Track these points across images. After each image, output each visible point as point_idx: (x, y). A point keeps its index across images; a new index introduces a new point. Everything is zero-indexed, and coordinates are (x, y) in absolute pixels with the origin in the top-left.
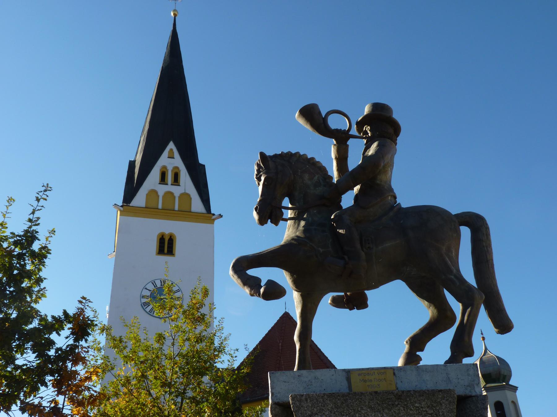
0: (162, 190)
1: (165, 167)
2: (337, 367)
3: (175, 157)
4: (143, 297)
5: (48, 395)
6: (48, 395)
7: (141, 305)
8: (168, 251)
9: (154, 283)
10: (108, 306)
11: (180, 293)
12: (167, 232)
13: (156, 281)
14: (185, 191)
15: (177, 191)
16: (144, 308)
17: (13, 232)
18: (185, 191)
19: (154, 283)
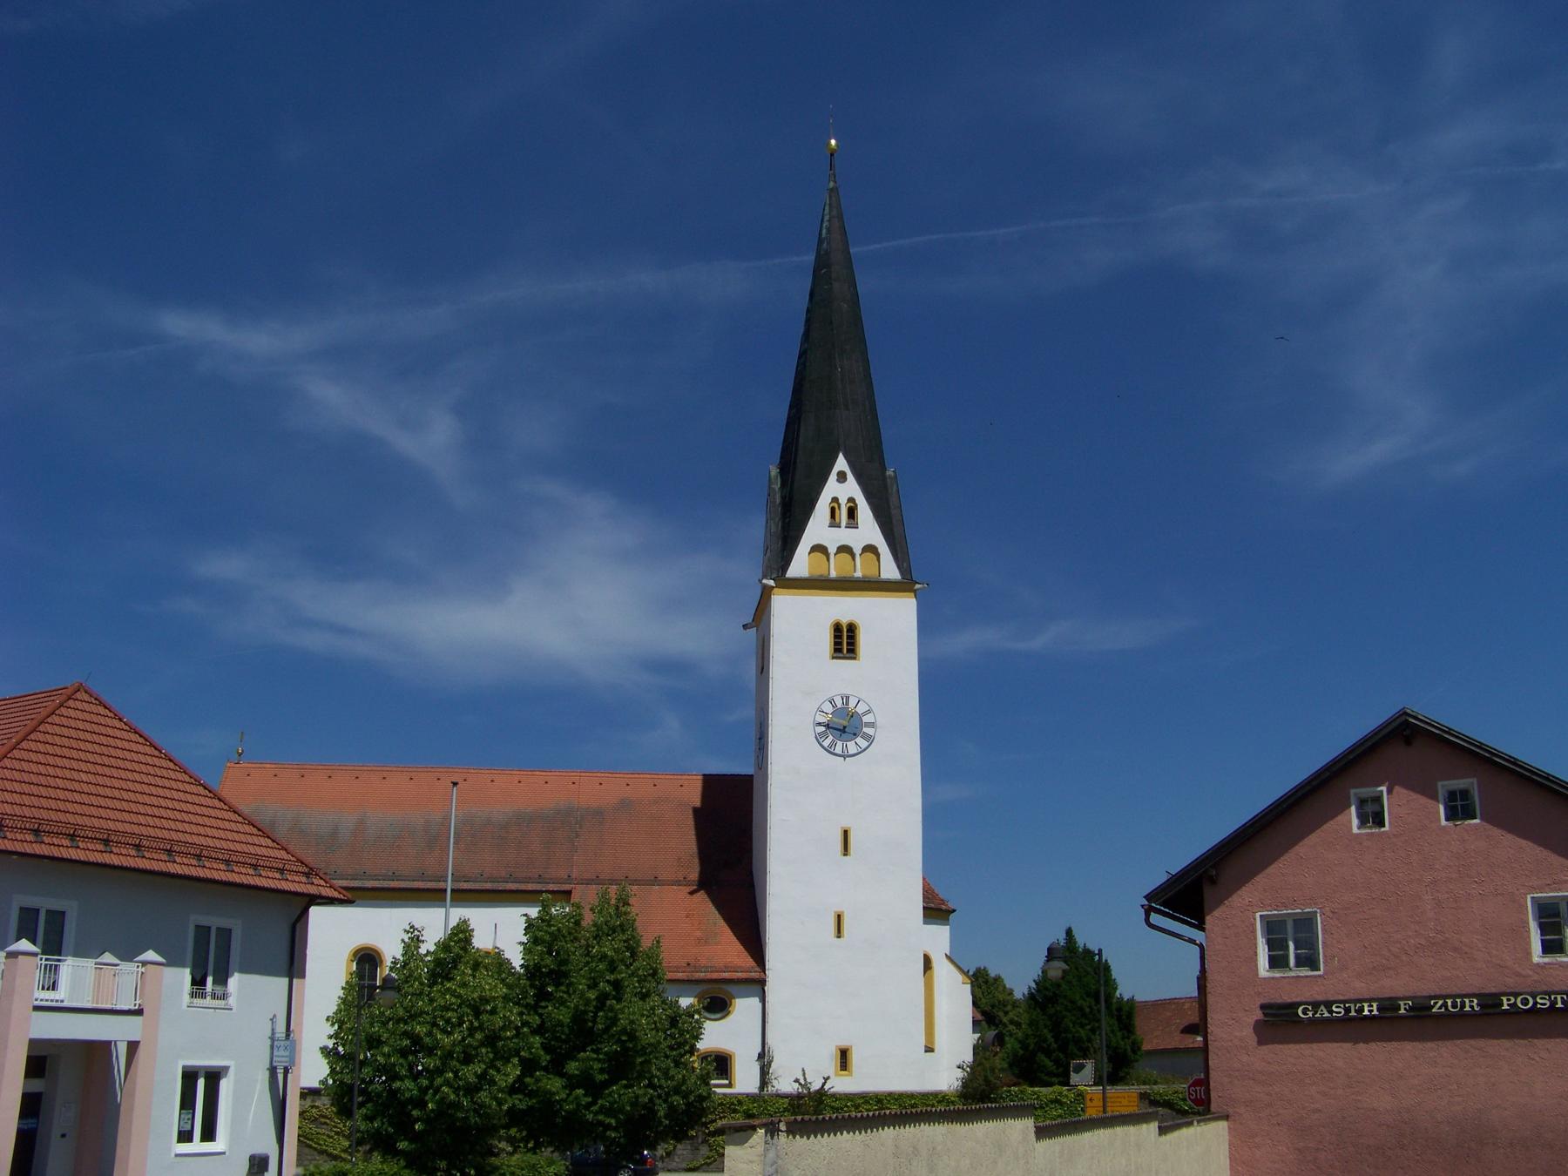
7: (816, 737)
8: (848, 651)
12: (844, 621)
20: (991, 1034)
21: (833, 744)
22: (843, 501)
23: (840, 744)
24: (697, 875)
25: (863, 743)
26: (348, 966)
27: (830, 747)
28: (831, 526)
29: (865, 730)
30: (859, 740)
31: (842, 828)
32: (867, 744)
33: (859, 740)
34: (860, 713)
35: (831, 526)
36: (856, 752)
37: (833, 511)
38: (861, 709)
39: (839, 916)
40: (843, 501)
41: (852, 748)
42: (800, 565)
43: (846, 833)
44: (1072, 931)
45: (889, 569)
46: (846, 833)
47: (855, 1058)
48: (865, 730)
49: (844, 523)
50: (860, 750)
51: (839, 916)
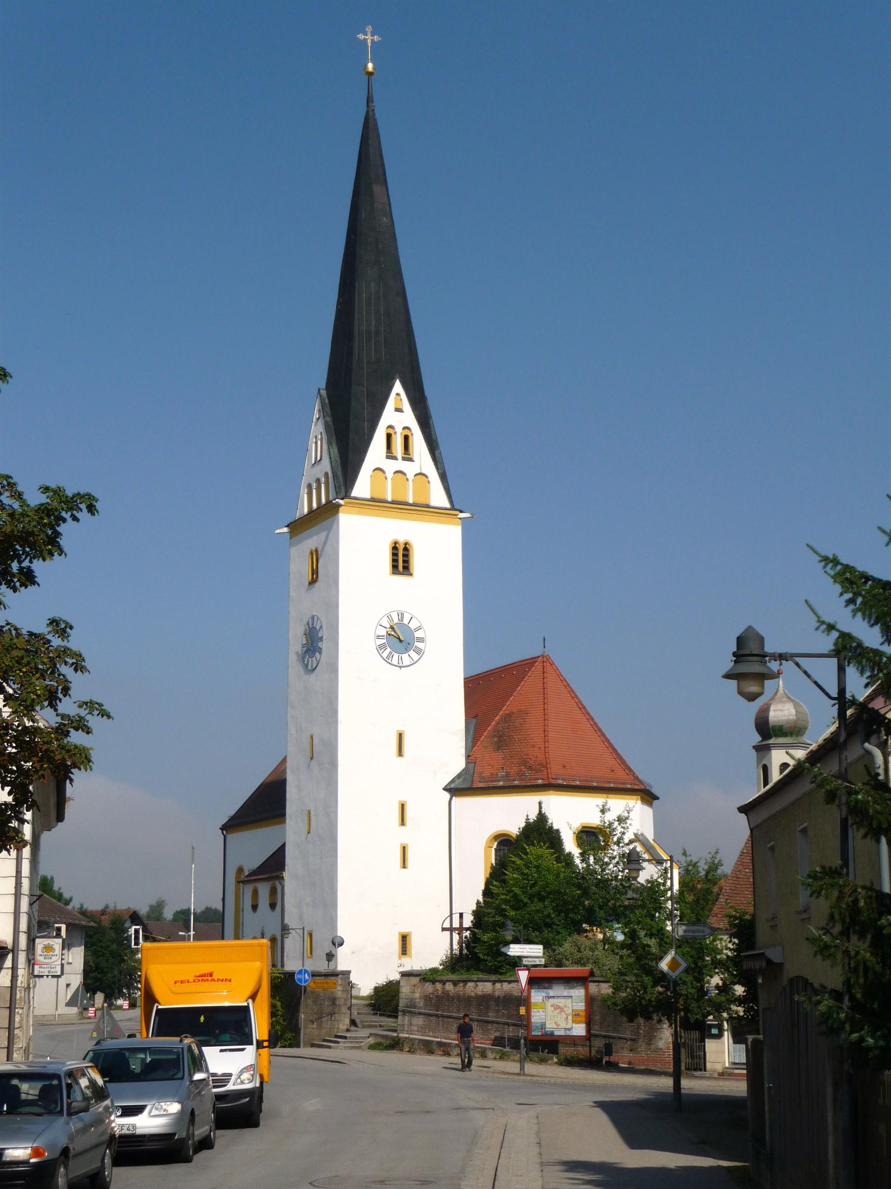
0: (390, 467)
1: (390, 427)
2: (765, 687)
3: (404, 410)
4: (379, 637)
5: (174, 993)
6: (174, 993)
7: (377, 648)
8: (404, 567)
9: (419, 628)
10: (36, 1152)
11: (392, 614)
12: (402, 540)
13: (392, 614)
14: (421, 470)
15: (410, 469)
16: (381, 652)
17: (7, 587)
18: (421, 470)
19: (419, 628)
20: (630, 941)
21: (390, 656)
22: (399, 429)
23: (396, 655)
24: (583, 1004)
25: (415, 656)
26: (487, 857)
27: (388, 657)
28: (388, 457)
29: (417, 644)
30: (412, 653)
31: (401, 844)
32: (418, 657)
33: (412, 653)
34: (413, 629)
35: (388, 457)
36: (410, 664)
37: (389, 436)
38: (413, 625)
39: (404, 848)
40: (399, 429)
41: (406, 659)
42: (362, 487)
43: (404, 849)
44: (742, 807)
45: (438, 497)
46: (404, 849)
47: (414, 943)
48: (417, 644)
49: (400, 456)
50: (413, 662)
51: (404, 848)
